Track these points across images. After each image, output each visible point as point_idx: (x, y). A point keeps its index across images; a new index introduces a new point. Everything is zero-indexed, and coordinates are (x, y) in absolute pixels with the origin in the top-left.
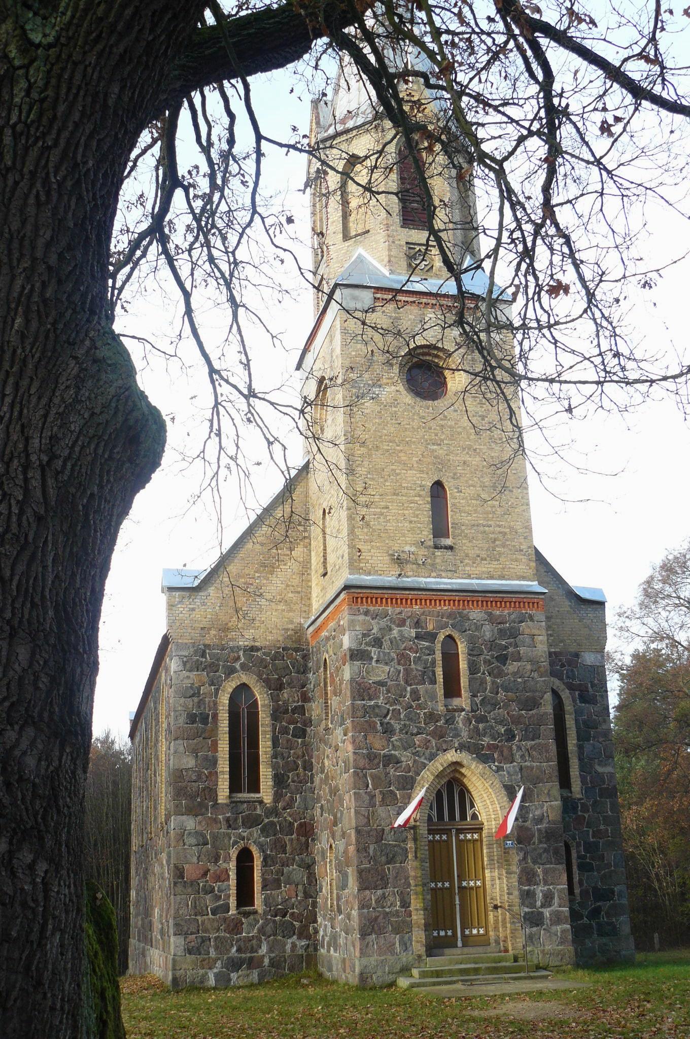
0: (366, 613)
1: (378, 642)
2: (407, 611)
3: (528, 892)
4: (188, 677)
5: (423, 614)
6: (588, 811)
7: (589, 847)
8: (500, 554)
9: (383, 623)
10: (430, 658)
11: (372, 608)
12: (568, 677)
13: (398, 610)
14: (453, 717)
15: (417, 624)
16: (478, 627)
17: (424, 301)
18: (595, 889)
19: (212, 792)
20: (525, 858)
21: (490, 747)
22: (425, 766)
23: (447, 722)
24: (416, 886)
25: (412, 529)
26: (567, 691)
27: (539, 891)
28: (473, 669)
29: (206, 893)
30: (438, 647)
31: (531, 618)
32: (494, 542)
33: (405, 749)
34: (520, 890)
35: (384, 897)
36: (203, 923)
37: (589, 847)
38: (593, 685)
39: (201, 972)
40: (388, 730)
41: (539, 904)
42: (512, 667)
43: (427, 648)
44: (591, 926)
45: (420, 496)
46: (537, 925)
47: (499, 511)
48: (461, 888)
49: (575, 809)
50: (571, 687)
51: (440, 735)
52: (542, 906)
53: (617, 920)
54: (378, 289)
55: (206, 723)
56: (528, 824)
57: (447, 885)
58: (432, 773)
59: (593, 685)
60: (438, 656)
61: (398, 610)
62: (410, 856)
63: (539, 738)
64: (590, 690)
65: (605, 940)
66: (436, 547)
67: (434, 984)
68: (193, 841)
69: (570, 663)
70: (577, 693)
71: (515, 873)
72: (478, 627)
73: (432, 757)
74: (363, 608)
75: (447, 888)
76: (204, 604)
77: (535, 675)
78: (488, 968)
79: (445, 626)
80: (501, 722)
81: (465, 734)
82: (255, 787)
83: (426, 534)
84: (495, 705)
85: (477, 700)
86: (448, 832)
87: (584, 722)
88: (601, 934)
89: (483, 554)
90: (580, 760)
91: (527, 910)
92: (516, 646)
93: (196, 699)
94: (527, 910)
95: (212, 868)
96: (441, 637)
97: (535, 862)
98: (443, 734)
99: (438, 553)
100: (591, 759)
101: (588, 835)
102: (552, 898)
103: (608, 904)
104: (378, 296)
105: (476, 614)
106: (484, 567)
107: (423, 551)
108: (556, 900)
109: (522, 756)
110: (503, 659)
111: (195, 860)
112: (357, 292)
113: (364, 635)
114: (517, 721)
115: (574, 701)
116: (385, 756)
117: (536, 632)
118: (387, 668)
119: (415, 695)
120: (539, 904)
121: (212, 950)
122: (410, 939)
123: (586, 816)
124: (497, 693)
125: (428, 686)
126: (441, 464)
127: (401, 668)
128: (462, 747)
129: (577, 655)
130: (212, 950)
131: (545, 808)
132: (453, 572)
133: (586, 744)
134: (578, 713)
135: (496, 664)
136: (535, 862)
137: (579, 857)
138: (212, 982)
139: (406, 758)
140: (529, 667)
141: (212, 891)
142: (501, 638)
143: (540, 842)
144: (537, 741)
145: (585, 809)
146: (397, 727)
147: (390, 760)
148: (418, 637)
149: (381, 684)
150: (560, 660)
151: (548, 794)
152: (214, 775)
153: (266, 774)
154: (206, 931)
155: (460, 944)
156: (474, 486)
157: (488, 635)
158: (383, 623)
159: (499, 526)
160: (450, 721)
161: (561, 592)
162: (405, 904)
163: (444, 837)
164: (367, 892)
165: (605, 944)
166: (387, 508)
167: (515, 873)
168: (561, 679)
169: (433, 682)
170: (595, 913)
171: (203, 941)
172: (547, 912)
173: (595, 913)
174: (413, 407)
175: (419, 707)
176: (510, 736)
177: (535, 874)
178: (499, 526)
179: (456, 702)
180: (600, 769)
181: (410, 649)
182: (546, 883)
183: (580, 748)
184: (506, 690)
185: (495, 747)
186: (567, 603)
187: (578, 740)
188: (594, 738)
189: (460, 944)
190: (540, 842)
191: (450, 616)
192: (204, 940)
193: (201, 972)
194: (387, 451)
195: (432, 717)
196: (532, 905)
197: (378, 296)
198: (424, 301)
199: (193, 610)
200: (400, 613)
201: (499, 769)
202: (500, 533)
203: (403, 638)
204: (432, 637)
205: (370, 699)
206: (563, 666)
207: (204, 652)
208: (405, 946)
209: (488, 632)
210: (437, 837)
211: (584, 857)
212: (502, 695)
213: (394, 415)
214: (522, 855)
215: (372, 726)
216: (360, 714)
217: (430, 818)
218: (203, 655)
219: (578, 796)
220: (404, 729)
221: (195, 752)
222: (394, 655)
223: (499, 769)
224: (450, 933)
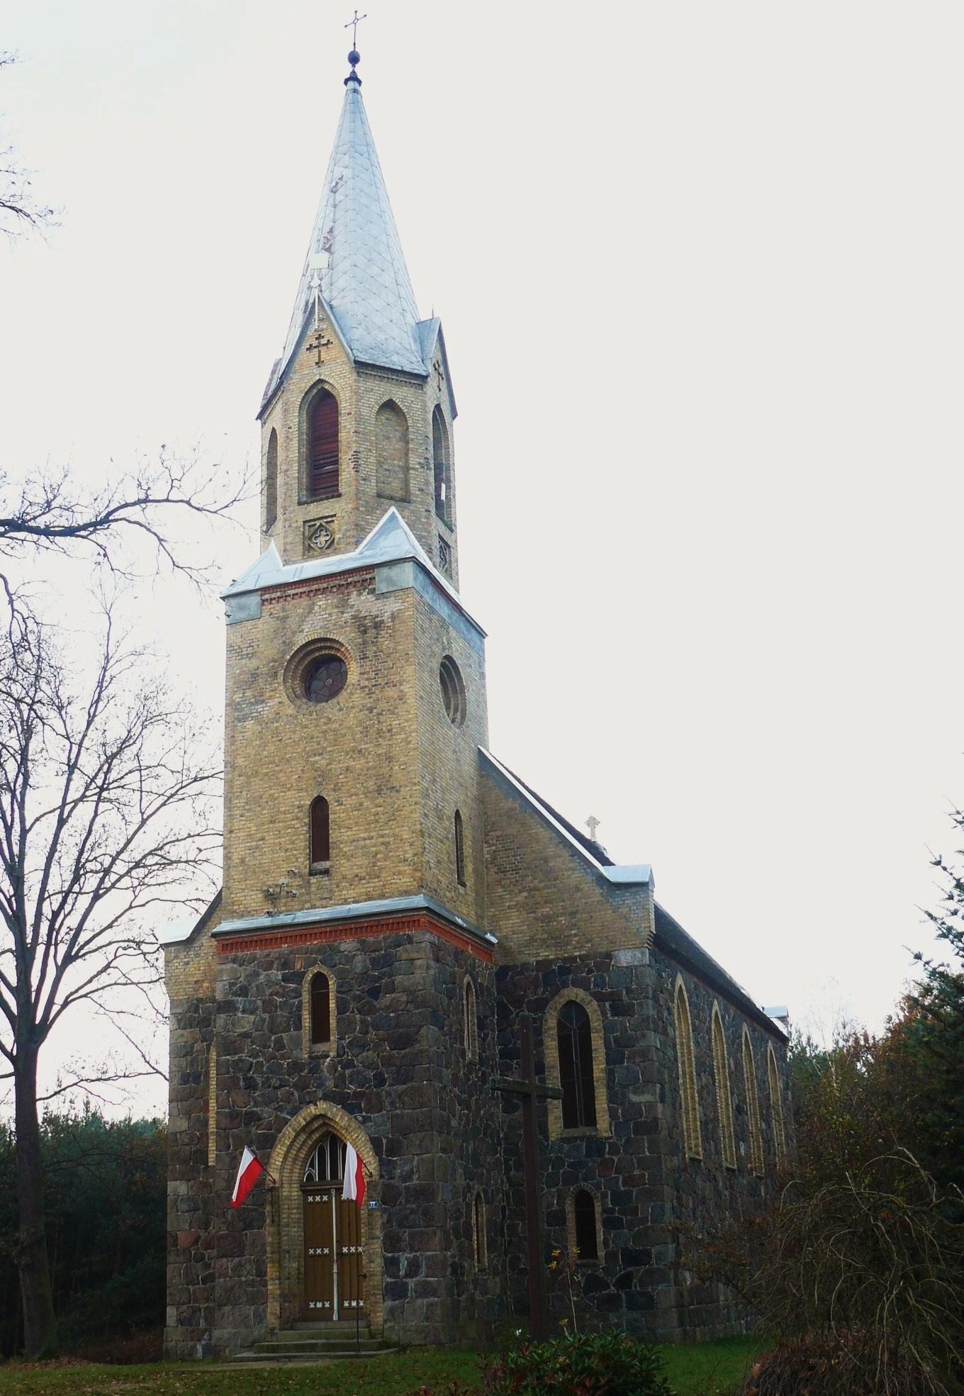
0: (234, 961)
1: (244, 991)
2: (274, 951)
3: (393, 1258)
4: (182, 1035)
5: (291, 953)
6: (619, 1152)
7: (618, 1198)
8: (381, 869)
9: (250, 969)
10: (296, 1001)
11: (240, 954)
12: (596, 985)
13: (266, 952)
14: (318, 1065)
15: (285, 964)
16: (350, 959)
17: (316, 587)
18: (626, 1252)
19: (204, 1154)
20: (389, 1221)
21: (356, 1095)
22: (286, 1121)
23: (311, 1071)
24: (272, 1253)
25: (288, 858)
26: (595, 1003)
27: (404, 1258)
28: (342, 1008)
29: (197, 1262)
30: (306, 986)
31: (410, 940)
32: (374, 856)
33: (267, 1105)
34: (385, 1258)
35: (240, 1265)
36: (194, 1292)
37: (618, 1198)
38: (629, 991)
39: (191, 1343)
40: (251, 1085)
41: (402, 1273)
42: (387, 999)
43: (294, 990)
44: (618, 1296)
45: (297, 818)
46: (400, 1298)
47: (383, 818)
48: (340, 1254)
49: (600, 1152)
50: (599, 998)
51: (302, 1086)
52: (406, 1276)
53: (654, 1290)
54: (265, 590)
55: (198, 1083)
56: (395, 1182)
57: (326, 1251)
58: (294, 1130)
59: (629, 991)
60: (306, 997)
61: (266, 952)
62: (268, 1221)
63: (411, 1080)
64: (625, 998)
65: (635, 1315)
66: (312, 873)
67: (256, 1360)
68: (184, 1207)
69: (599, 966)
70: (607, 1004)
71: (378, 1238)
72: (350, 959)
73: (294, 1112)
74: (231, 955)
75: (326, 1255)
76: (197, 955)
77: (410, 1007)
78: (324, 1345)
79: (314, 963)
80: (369, 1066)
81: (330, 1084)
82: (592, 1121)
83: (302, 862)
84: (364, 1047)
85: (345, 1042)
86: (327, 1192)
87: (616, 1040)
88: (632, 1306)
89: (362, 872)
90: (610, 1088)
91: (389, 1280)
92: (390, 976)
93: (189, 1058)
94: (389, 1280)
95: (202, 1234)
96: (309, 976)
97: (400, 1225)
98: (305, 1081)
99: (313, 880)
100: (626, 1087)
101: (617, 1183)
102: (419, 1267)
103: (642, 1269)
104: (267, 596)
105: (348, 945)
106: (361, 889)
107: (298, 881)
108: (424, 1269)
109: (392, 1104)
110: (375, 993)
111: (187, 1227)
112: (243, 600)
113: (231, 985)
114: (388, 1062)
115: (604, 1014)
116: (246, 1113)
117: (415, 956)
118: (252, 1017)
119: (280, 1045)
120: (402, 1273)
121: (202, 1321)
122: (265, 1311)
123: (616, 1159)
124: (367, 1033)
125: (293, 1032)
126: (323, 776)
127: (266, 1016)
128: (326, 1098)
129: (609, 956)
130: (202, 1321)
131: (415, 1163)
132: (327, 900)
133: (618, 1068)
134: (608, 1029)
135: (368, 999)
136: (400, 1225)
137: (605, 1211)
138: (200, 1354)
139: (267, 1112)
140: (404, 998)
141: (203, 1258)
142: (373, 969)
143: (408, 1202)
144: (409, 1084)
145: (614, 1149)
146: (259, 1080)
147: (252, 1118)
148: (286, 979)
149: (245, 1035)
150: (587, 966)
151: (420, 1146)
152: (205, 1136)
153: (601, 1103)
154: (196, 1301)
155: (335, 1317)
156: (357, 795)
157: (359, 967)
158: (250, 969)
159: (382, 836)
160: (315, 1069)
161: (590, 878)
162: (261, 1273)
163: (325, 1198)
164: (225, 1260)
165: (635, 1320)
166: (263, 839)
167: (378, 1238)
168: (587, 989)
169: (299, 1027)
170: (625, 1282)
171: (194, 1312)
172: (411, 1283)
173: (625, 1282)
174: (296, 717)
175: (283, 1057)
176: (380, 1081)
177: (399, 1240)
178: (382, 836)
179: (321, 1048)
180: (635, 1099)
181: (277, 994)
182: (412, 1250)
183: (610, 1074)
184: (377, 1028)
185: (362, 1095)
186: (598, 891)
187: (608, 1063)
188: (629, 1059)
189: (335, 1317)
190: (408, 1202)
191: (319, 951)
192: (195, 1311)
193: (191, 1343)
194: (266, 774)
195: (296, 1067)
196: (394, 1275)
197: (267, 596)
198: (316, 587)
199: (187, 963)
200: (268, 955)
201: (366, 1120)
202: (383, 843)
203: (270, 983)
204: (298, 977)
205: (236, 1053)
206: (590, 971)
207: (197, 1006)
208: (260, 1318)
209: (359, 963)
210: (318, 1198)
211: (611, 1211)
212: (372, 1035)
213: (276, 733)
214: (385, 1217)
215: (235, 1080)
216: (224, 1070)
217: (310, 1177)
218: (196, 1011)
219: (605, 1135)
220: (266, 1083)
221: (188, 1114)
222: (259, 1003)
223: (366, 1120)
224: (327, 1305)
